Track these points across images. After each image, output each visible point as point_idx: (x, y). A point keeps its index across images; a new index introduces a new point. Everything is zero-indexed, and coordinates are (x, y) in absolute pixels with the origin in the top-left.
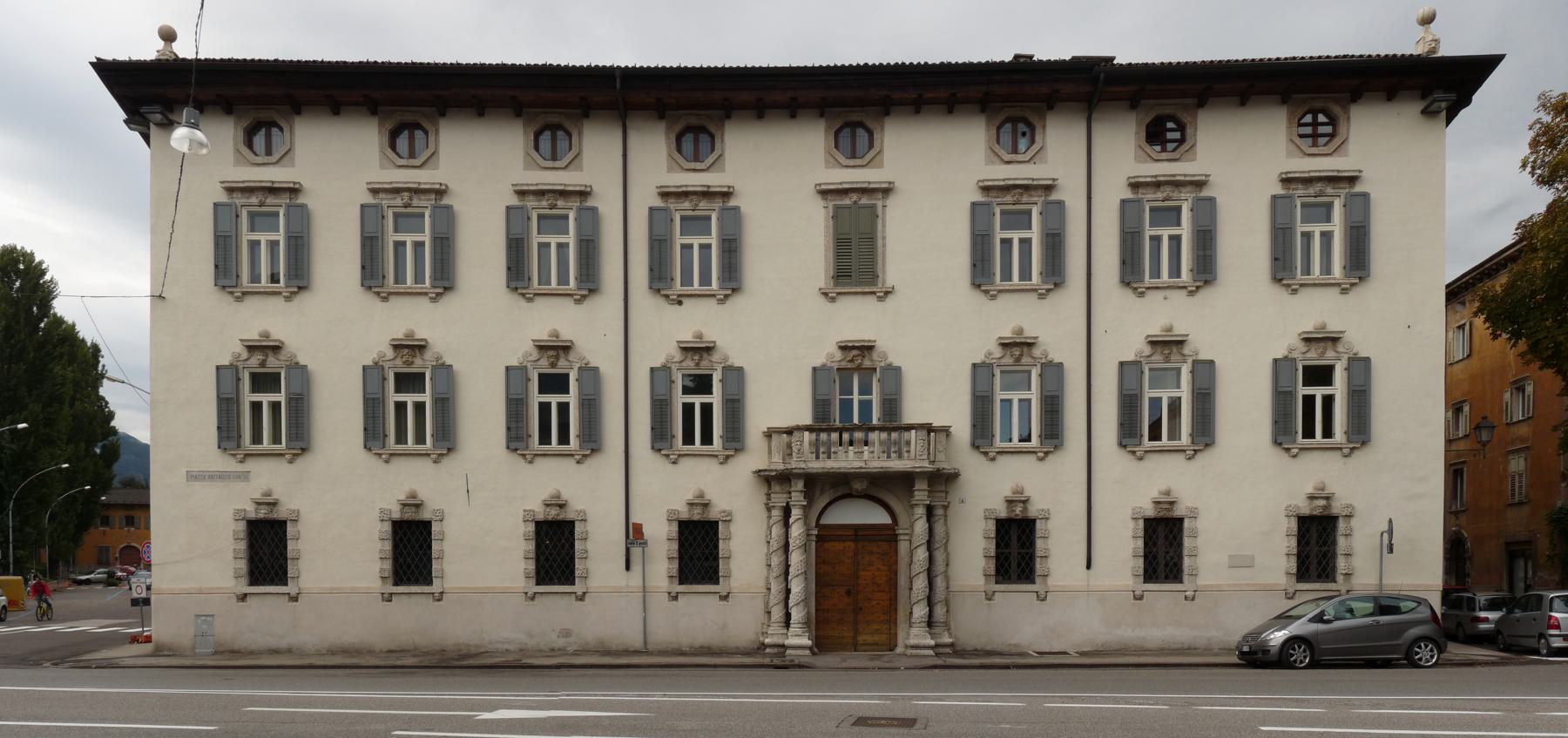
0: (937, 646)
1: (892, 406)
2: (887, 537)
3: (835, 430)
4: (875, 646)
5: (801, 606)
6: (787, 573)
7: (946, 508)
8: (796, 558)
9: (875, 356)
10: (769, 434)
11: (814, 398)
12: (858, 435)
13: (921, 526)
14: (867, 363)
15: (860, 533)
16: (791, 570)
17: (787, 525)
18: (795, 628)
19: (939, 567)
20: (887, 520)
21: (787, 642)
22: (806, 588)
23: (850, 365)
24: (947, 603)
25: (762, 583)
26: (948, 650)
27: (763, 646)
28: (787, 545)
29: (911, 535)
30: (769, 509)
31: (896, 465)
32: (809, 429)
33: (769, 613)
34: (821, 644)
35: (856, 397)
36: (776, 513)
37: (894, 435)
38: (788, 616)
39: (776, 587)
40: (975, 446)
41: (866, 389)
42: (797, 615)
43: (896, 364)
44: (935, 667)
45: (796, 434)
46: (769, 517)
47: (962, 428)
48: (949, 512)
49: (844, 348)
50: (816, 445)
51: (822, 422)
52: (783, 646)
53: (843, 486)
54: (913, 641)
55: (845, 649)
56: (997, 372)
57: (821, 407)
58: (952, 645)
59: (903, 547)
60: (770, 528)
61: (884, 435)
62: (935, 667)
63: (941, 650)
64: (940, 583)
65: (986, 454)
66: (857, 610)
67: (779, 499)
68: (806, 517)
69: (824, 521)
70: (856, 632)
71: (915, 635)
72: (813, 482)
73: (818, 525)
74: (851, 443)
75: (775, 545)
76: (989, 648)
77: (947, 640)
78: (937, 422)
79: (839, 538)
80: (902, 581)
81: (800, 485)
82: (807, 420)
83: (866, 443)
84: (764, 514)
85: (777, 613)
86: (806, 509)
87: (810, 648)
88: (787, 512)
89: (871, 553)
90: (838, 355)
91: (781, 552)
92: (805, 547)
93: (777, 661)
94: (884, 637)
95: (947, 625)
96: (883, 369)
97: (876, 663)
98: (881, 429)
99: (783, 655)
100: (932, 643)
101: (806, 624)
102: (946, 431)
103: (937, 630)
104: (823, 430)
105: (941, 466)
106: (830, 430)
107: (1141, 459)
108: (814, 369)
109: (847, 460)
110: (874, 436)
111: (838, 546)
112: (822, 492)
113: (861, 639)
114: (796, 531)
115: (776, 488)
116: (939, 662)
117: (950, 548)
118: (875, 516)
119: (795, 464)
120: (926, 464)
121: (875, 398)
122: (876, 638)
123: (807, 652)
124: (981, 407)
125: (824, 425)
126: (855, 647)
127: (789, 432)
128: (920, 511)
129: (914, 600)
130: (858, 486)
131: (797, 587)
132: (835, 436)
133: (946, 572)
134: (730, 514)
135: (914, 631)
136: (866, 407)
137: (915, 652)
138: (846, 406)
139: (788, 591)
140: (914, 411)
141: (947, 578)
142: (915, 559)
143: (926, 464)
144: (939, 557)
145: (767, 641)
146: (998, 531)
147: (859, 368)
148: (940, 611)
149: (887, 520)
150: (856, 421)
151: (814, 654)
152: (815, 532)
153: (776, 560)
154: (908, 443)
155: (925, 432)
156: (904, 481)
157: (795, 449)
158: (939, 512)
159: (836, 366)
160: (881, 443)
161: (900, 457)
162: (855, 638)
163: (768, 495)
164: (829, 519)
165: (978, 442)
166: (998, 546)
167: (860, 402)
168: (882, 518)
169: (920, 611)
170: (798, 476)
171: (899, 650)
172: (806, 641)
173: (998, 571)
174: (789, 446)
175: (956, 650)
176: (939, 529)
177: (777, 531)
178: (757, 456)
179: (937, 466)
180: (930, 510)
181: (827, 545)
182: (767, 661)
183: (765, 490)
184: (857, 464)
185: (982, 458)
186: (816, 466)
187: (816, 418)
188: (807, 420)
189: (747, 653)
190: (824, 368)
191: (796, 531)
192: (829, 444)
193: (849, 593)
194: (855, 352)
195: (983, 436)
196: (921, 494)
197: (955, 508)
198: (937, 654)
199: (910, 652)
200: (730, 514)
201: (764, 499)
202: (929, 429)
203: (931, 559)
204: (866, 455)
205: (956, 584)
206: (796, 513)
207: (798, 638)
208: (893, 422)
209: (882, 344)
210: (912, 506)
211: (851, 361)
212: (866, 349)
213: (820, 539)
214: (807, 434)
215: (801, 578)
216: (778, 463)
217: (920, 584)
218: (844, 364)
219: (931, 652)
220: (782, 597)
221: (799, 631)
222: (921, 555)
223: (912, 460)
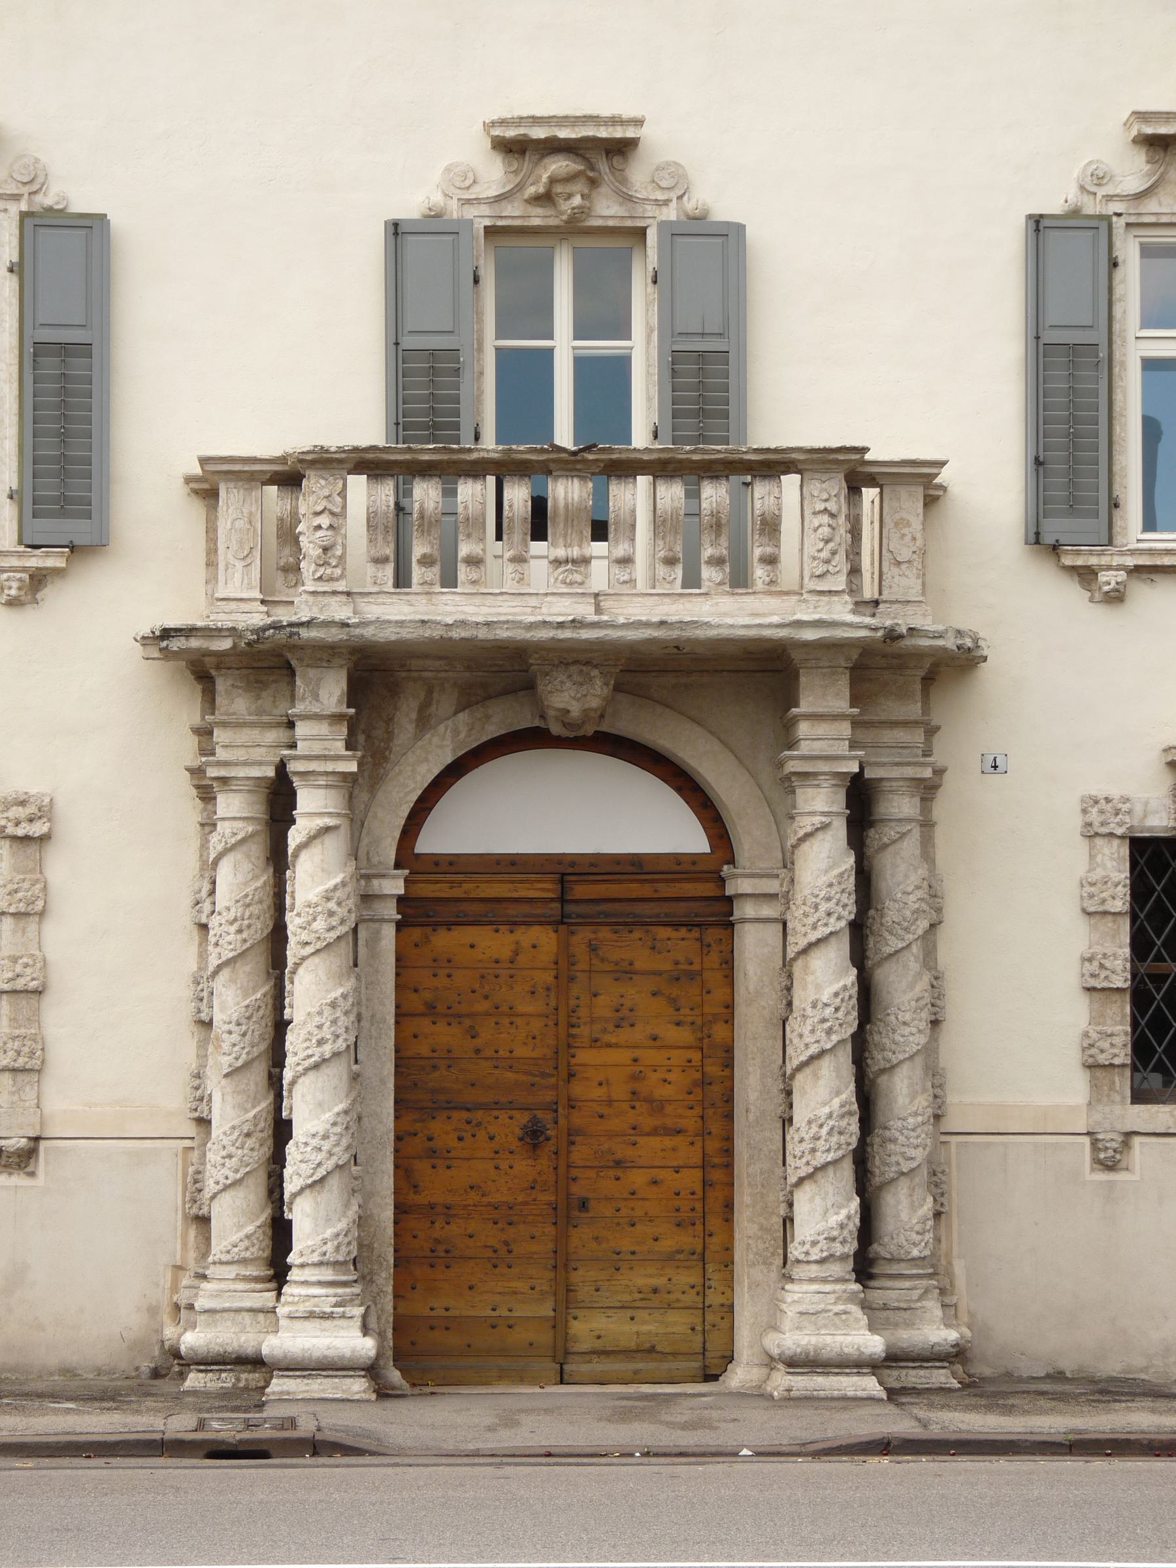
0: (894, 1358)
1: (706, 378)
2: (691, 905)
3: (476, 470)
4: (642, 1361)
5: (334, 1192)
6: (277, 1056)
7: (927, 790)
8: (313, 991)
9: (639, 175)
10: (208, 485)
11: (395, 344)
12: (567, 492)
13: (823, 864)
14: (607, 209)
15: (577, 891)
16: (293, 1040)
17: (278, 859)
18: (302, 1288)
19: (902, 1029)
20: (681, 834)
21: (273, 1345)
22: (356, 1120)
23: (537, 217)
24: (936, 1181)
25: (174, 1100)
26: (941, 1377)
27: (175, 1363)
28: (278, 936)
29: (785, 898)
30: (206, 794)
31: (726, 613)
32: (368, 463)
33: (203, 1221)
34: (420, 1355)
35: (564, 346)
36: (237, 810)
37: (714, 494)
38: (280, 1233)
39: (233, 1113)
40: (1042, 543)
41: (603, 315)
42: (315, 1227)
43: (723, 212)
44: (884, 1447)
45: (316, 485)
46: (208, 825)
47: (990, 476)
48: (941, 809)
49: (515, 148)
50: (399, 523)
51: (421, 445)
52: (256, 1362)
53: (510, 698)
54: (794, 1338)
55: (521, 1378)
56: (1129, 250)
57: (422, 379)
58: (957, 1355)
59: (754, 947)
60: (209, 868)
61: (672, 493)
62: (884, 1447)
63: (914, 1377)
64: (903, 1095)
65: (1086, 575)
66: (570, 1209)
67: (248, 753)
68: (356, 820)
69: (429, 843)
70: (566, 1300)
71: (798, 1313)
72: (378, 678)
73: (406, 856)
74: (539, 526)
75: (228, 938)
76: (1112, 1367)
77: (936, 1333)
78: (883, 450)
79: (494, 914)
80: (752, 1087)
81: (329, 691)
82: (365, 423)
83: (600, 531)
84: (190, 810)
85: (236, 1223)
86: (358, 790)
87: (371, 1370)
88: (279, 799)
89: (625, 973)
90: (493, 175)
91: (254, 967)
92: (353, 944)
93: (224, 1427)
94: (678, 1323)
95: (936, 1272)
96: (673, 233)
97: (640, 1433)
98: (662, 468)
99: (255, 1399)
100: (874, 1344)
101: (357, 1264)
102: (921, 481)
103: (888, 1293)
104: (425, 470)
105: (902, 620)
106: (452, 470)
107: (1115, 598)
108: (396, 229)
109: (520, 594)
110: (635, 498)
111: (492, 943)
112: (424, 723)
113: (586, 1328)
114: (316, 877)
115: (235, 702)
116: (898, 1423)
117: (944, 956)
118: (642, 822)
119: (309, 606)
120: (841, 610)
121: (642, 351)
122: (649, 1326)
123: (358, 1386)
124: (1066, 379)
125: (428, 451)
126: (562, 1364)
127: (289, 476)
128: (821, 803)
129: (798, 1167)
130: (568, 698)
131: (314, 1109)
132: (473, 494)
133: (930, 1052)
134: (45, 812)
135: (800, 1295)
136: (604, 383)
137: (803, 1383)
138: (525, 377)
139: (282, 1130)
140: (788, 406)
141: (935, 1079)
142: (801, 998)
143: (841, 610)
144: (902, 988)
145: (192, 1340)
146: (1139, 890)
147: (574, 229)
148: (905, 1214)
149: (681, 834)
150: (564, 435)
151: (384, 1393)
152: (395, 886)
153: (233, 1001)
154: (771, 526)
155: (836, 485)
156: (764, 673)
157: (310, 545)
158: (899, 806)
159: (481, 217)
160: (660, 524)
161: (739, 580)
162: (559, 1325)
163: (204, 733)
164: (459, 830)
165: (1054, 529)
166: (1140, 946)
167: (581, 364)
168: (670, 830)
169: (824, 1214)
170: (325, 654)
171: (739, 1376)
172: (366, 1346)
173: (1141, 1050)
174: (288, 534)
175: (969, 1372)
176: (900, 874)
177: (238, 879)
178: (167, 569)
179: (885, 619)
180: (861, 802)
181: (445, 941)
182: (180, 1425)
183: (190, 713)
184: (562, 609)
185: (1072, 594)
186: (396, 613)
187: (402, 422)
188: (365, 423)
189: (105, 1395)
190: (435, 226)
191: (316, 877)
192: (448, 528)
193: (534, 1136)
194: (559, 165)
195: (1074, 506)
196: (824, 733)
197: (964, 790)
198: (894, 1394)
199: (781, 1381)
200: (45, 812)
201: (187, 749)
202: (854, 472)
203: (865, 880)
204: (599, 575)
205: (969, 1104)
206: (313, 805)
207: (322, 1327)
208: (711, 447)
209: (661, 140)
210: (788, 784)
211: (546, 199)
212: (606, 152)
213: (414, 913)
214: (358, 484)
215: (335, 1076)
216: (237, 604)
217: (824, 1098)
218: (514, 213)
219: (870, 1385)
220: (257, 1152)
221: (325, 1299)
222: (827, 979)
223: (791, 594)
